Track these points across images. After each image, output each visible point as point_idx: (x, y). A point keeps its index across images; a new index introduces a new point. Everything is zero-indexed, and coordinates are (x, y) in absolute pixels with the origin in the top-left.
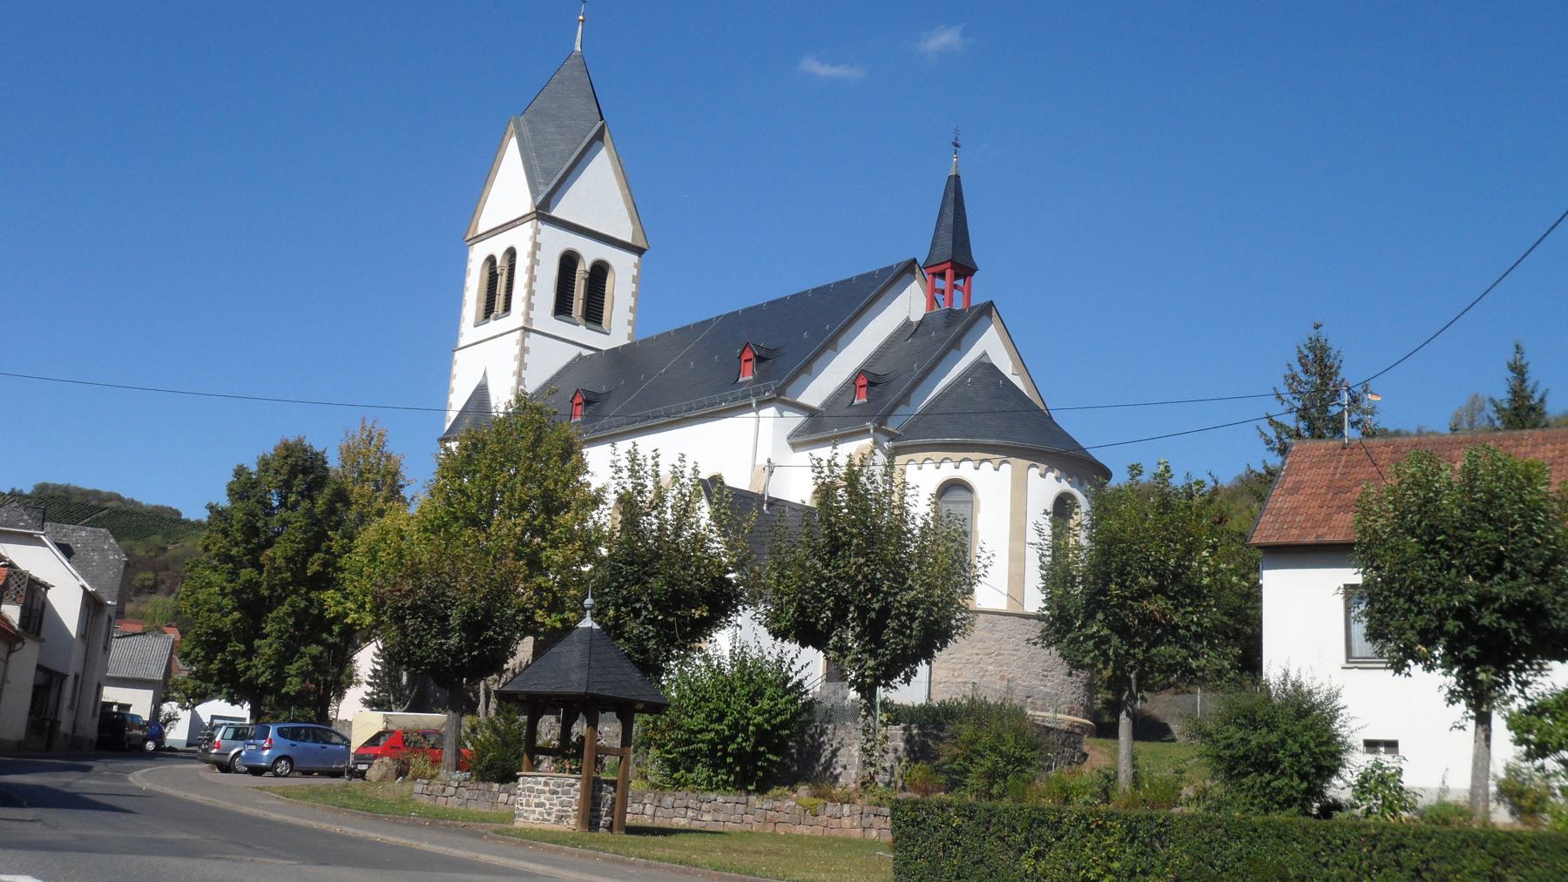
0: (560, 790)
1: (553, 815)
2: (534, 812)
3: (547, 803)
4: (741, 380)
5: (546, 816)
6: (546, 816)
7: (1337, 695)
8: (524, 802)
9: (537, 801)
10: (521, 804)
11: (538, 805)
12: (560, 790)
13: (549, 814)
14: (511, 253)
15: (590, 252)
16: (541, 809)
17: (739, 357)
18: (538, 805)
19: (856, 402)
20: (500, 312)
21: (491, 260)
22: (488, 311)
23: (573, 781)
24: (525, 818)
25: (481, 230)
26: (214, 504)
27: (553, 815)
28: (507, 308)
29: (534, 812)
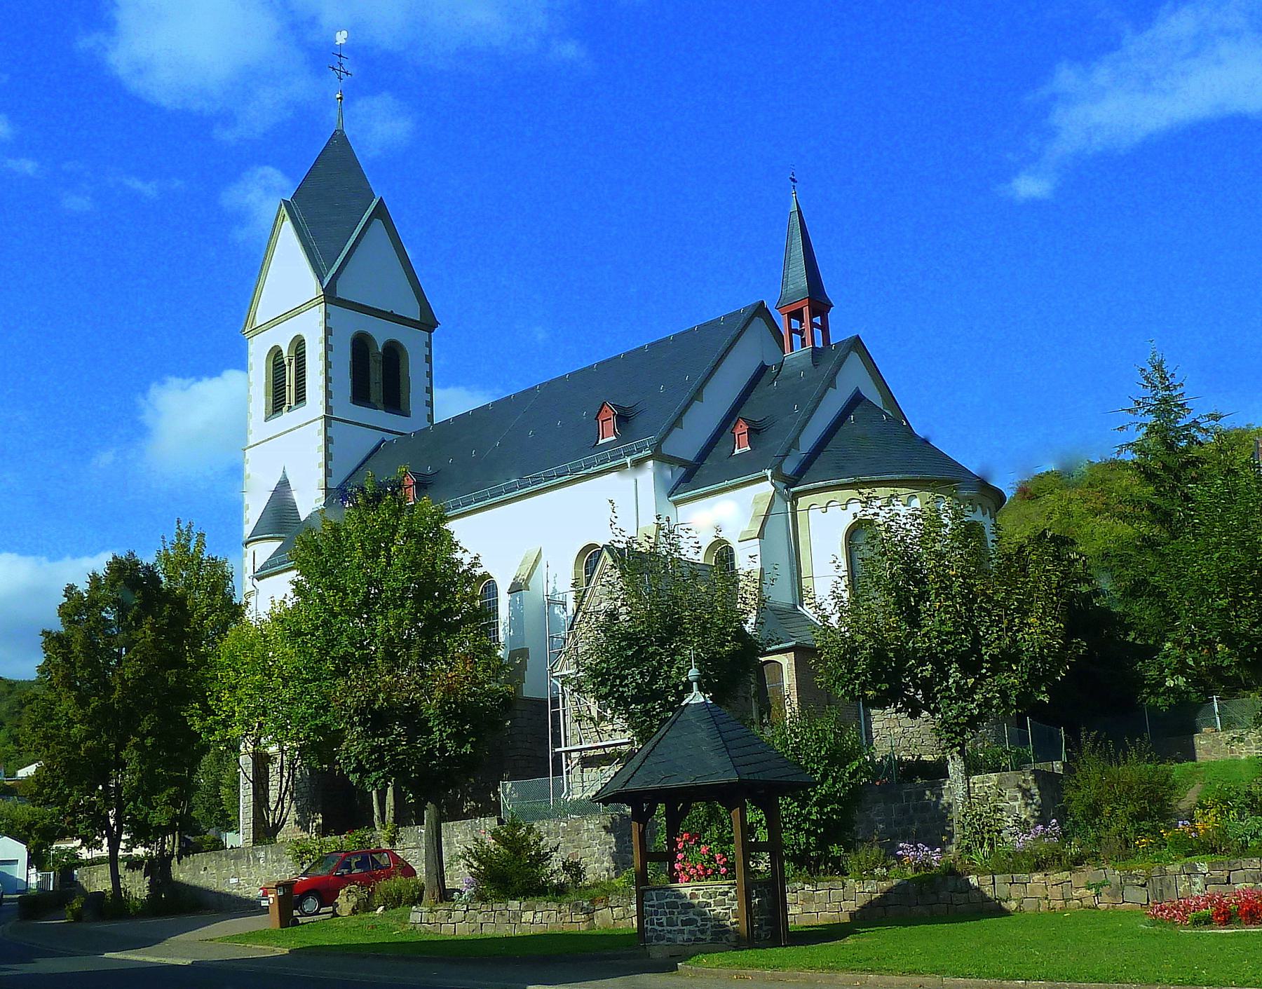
0: (711, 901)
1: (709, 933)
2: (682, 932)
3: (699, 919)
4: (601, 442)
5: (699, 935)
6: (699, 935)
7: (46, 634)
8: (664, 920)
9: (683, 917)
10: (661, 924)
11: (684, 923)
12: (711, 901)
13: (702, 932)
14: (299, 345)
15: (381, 333)
16: (692, 928)
17: (596, 419)
18: (684, 923)
19: (737, 451)
20: (293, 404)
21: (276, 352)
22: (277, 404)
23: (726, 888)
24: (669, 940)
25: (258, 323)
26: (48, 630)
27: (709, 933)
28: (301, 398)
29: (682, 932)
